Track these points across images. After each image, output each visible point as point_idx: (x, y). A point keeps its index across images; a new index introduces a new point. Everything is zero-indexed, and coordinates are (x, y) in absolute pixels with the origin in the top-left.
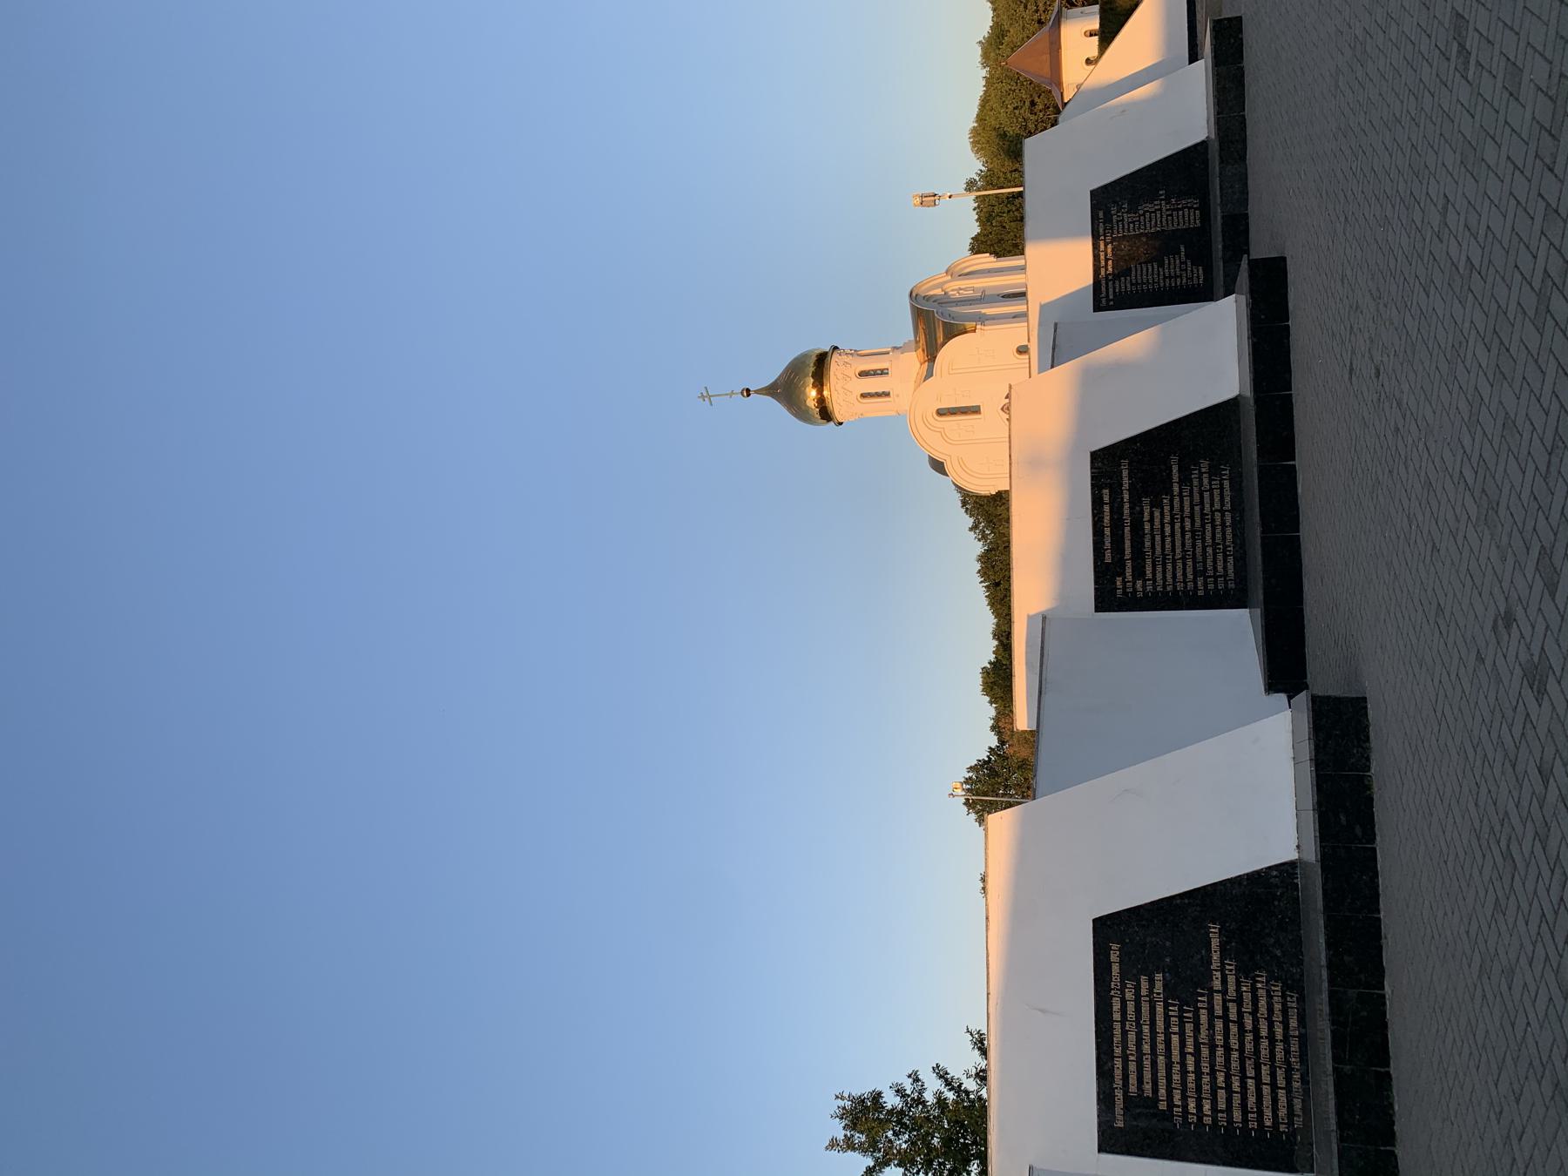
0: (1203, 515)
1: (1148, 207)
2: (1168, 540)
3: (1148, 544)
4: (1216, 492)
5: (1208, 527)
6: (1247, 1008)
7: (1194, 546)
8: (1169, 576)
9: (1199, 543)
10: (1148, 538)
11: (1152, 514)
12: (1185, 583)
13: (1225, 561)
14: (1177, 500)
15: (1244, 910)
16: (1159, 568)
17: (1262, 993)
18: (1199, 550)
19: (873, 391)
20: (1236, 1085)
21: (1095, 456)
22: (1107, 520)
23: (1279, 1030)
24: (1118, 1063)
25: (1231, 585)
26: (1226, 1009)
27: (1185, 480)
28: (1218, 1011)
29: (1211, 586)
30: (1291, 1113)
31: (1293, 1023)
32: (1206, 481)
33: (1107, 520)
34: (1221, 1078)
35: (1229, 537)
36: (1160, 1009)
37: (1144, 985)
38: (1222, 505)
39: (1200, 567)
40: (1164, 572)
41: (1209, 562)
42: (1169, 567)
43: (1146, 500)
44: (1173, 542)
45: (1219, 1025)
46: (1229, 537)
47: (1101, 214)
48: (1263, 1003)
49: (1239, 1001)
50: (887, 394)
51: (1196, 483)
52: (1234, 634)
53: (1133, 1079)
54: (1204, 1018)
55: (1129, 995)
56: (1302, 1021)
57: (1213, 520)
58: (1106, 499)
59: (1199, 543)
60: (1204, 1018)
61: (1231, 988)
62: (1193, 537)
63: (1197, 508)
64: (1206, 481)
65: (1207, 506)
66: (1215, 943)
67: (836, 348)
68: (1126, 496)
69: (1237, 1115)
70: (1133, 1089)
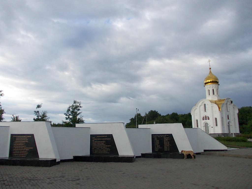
0: (103, 149)
1: (168, 143)
2: (99, 145)
3: (99, 142)
4: (106, 151)
5: (101, 150)
6: (24, 151)
7: (98, 148)
8: (95, 145)
9: (99, 149)
10: (100, 142)
11: (103, 142)
12: (94, 147)
13: (96, 152)
14: (105, 146)
15: (35, 152)
16: (96, 143)
17: (26, 153)
18: (98, 149)
19: (210, 93)
20: (17, 149)
21: (112, 135)
22: (103, 136)
23: (22, 155)
24: (19, 137)
25: (93, 153)
26: (24, 149)
27: (107, 147)
28: (24, 148)
29: (93, 150)
30: (14, 155)
31: (23, 156)
32: (107, 150)
33: (103, 136)
34: (18, 148)
35: (99, 153)
36: (24, 141)
37: (27, 140)
38: (104, 152)
39: (96, 149)
40: (95, 144)
41: (96, 150)
42: (96, 145)
43: (105, 142)
44: (99, 145)
45: (23, 148)
46: (99, 153)
47: (168, 135)
48: (25, 153)
49: (25, 150)
50: (209, 95)
51: (107, 149)
52: (86, 152)
53: (18, 138)
54: (23, 146)
55: (26, 138)
56: (23, 157)
57: (102, 151)
58: (106, 136)
59: (99, 149)
60: (23, 146)
61: (26, 150)
62: (100, 148)
63: (103, 149)
64: (107, 150)
65: (104, 150)
66: (31, 148)
67: (219, 85)
68: (106, 139)
69: (14, 149)
70: (17, 138)
